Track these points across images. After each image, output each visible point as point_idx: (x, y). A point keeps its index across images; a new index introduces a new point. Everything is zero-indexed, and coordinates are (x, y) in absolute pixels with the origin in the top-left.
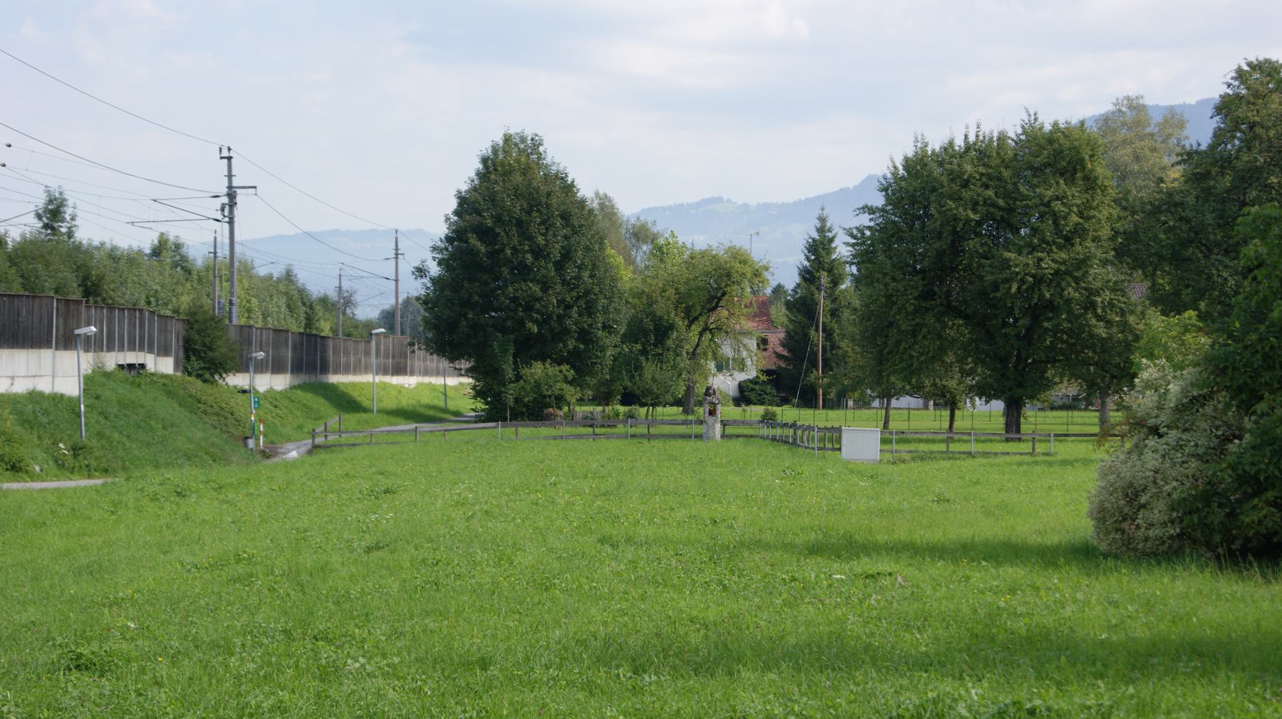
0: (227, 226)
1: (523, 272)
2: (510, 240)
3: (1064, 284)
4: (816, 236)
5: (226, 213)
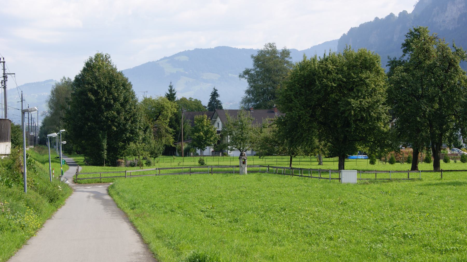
0: (3, 89)
1: (109, 107)
2: (104, 95)
3: (370, 111)
4: (169, 93)
5: (3, 84)
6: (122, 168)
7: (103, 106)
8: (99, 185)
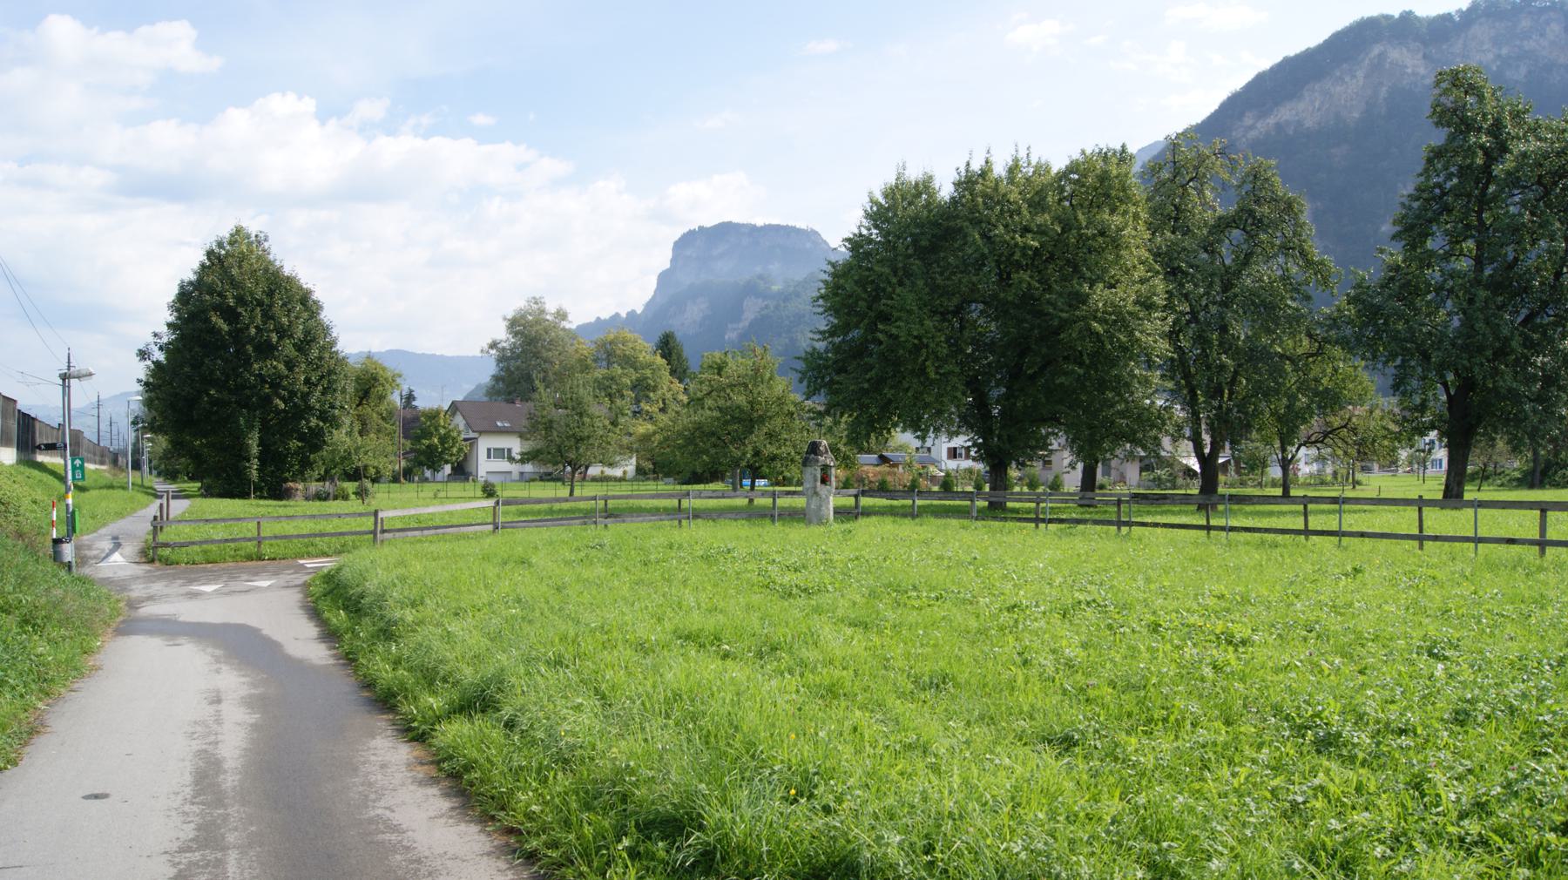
1: (266, 350)
2: (253, 321)
6: (298, 506)
7: (249, 348)
8: (256, 573)
